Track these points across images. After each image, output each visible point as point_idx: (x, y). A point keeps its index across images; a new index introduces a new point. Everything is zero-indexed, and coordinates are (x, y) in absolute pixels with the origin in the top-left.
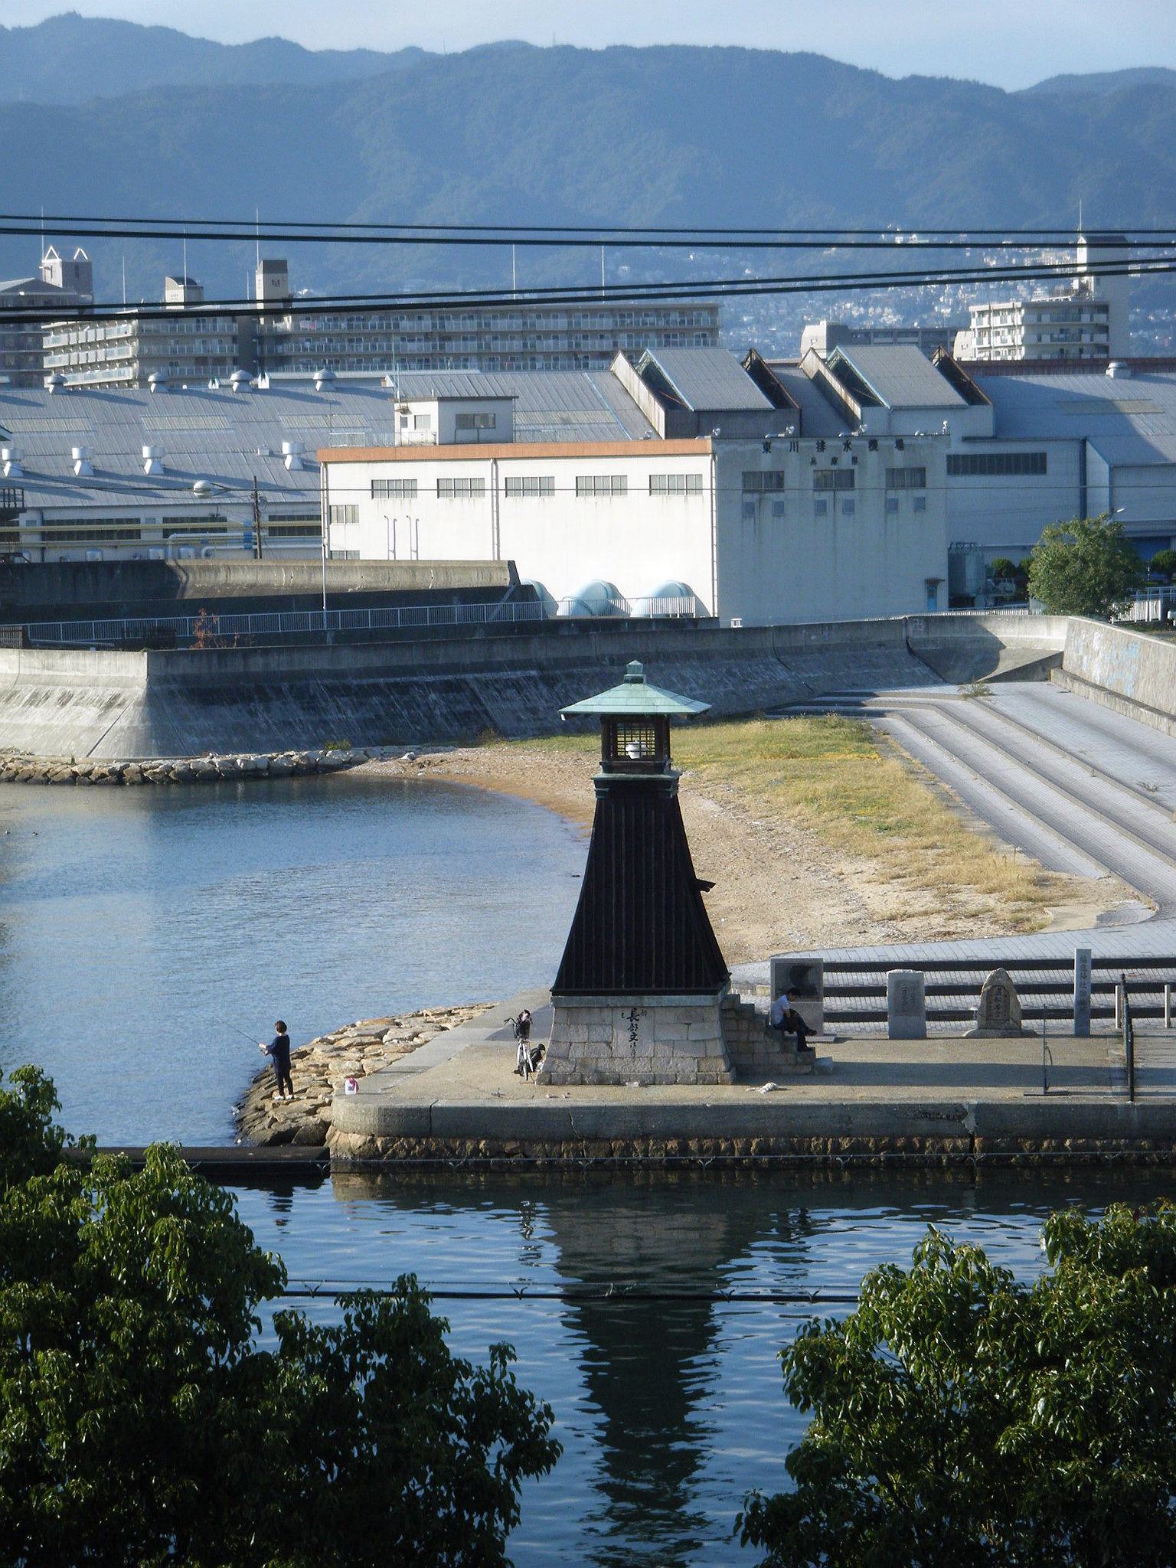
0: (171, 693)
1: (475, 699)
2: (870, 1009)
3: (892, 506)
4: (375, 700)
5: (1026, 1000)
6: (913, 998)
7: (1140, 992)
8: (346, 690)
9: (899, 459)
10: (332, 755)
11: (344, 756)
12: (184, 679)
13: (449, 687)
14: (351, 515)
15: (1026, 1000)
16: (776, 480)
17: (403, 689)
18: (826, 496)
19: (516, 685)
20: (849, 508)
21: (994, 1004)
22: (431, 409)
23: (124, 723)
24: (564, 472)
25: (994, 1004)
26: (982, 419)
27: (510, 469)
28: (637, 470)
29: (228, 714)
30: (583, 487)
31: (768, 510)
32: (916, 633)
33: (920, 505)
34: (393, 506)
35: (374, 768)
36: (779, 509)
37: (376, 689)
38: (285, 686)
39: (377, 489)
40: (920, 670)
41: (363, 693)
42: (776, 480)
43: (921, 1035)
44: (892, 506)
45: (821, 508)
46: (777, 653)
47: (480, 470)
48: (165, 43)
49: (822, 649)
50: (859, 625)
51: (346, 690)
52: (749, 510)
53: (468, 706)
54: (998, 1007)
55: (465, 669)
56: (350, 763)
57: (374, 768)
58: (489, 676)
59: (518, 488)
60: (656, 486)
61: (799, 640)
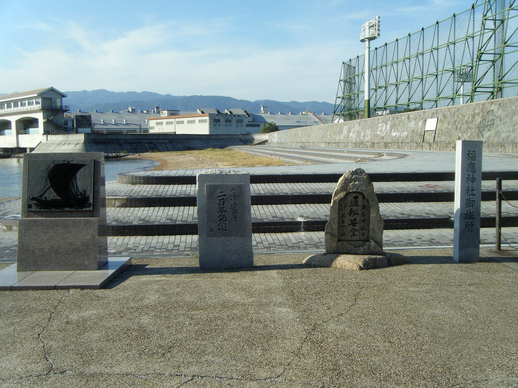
0: (89, 142)
1: (155, 145)
2: (276, 193)
3: (237, 126)
4: (134, 145)
5: (388, 209)
6: (235, 211)
7: (267, 204)
8: (128, 143)
9: (238, 118)
10: (122, 154)
11: (124, 155)
12: (92, 139)
13: (150, 143)
14: (153, 128)
15: (388, 209)
16: (219, 121)
17: (140, 143)
18: (227, 123)
19: (164, 143)
20: (231, 125)
21: (348, 220)
22: (166, 112)
23: (78, 148)
24: (186, 120)
25: (348, 220)
26: (251, 119)
27: (177, 120)
28: (197, 119)
29: (101, 146)
30: (188, 122)
31: (217, 126)
32: (241, 137)
33: (242, 126)
34: (159, 126)
35: (130, 156)
36: (219, 125)
37: (135, 143)
38: (115, 141)
39: (157, 124)
40: (242, 143)
41: (132, 143)
42: (219, 121)
43: (244, 264)
44: (237, 126)
45: (226, 125)
46: (215, 139)
47: (173, 120)
48: (156, 94)
49: (224, 139)
50: (231, 135)
51: (128, 143)
52: (215, 125)
53: (154, 147)
54: (353, 223)
55: (154, 140)
56: (126, 156)
57: (130, 156)
58: (158, 141)
59: (178, 123)
60: (200, 121)
61: (220, 137)
